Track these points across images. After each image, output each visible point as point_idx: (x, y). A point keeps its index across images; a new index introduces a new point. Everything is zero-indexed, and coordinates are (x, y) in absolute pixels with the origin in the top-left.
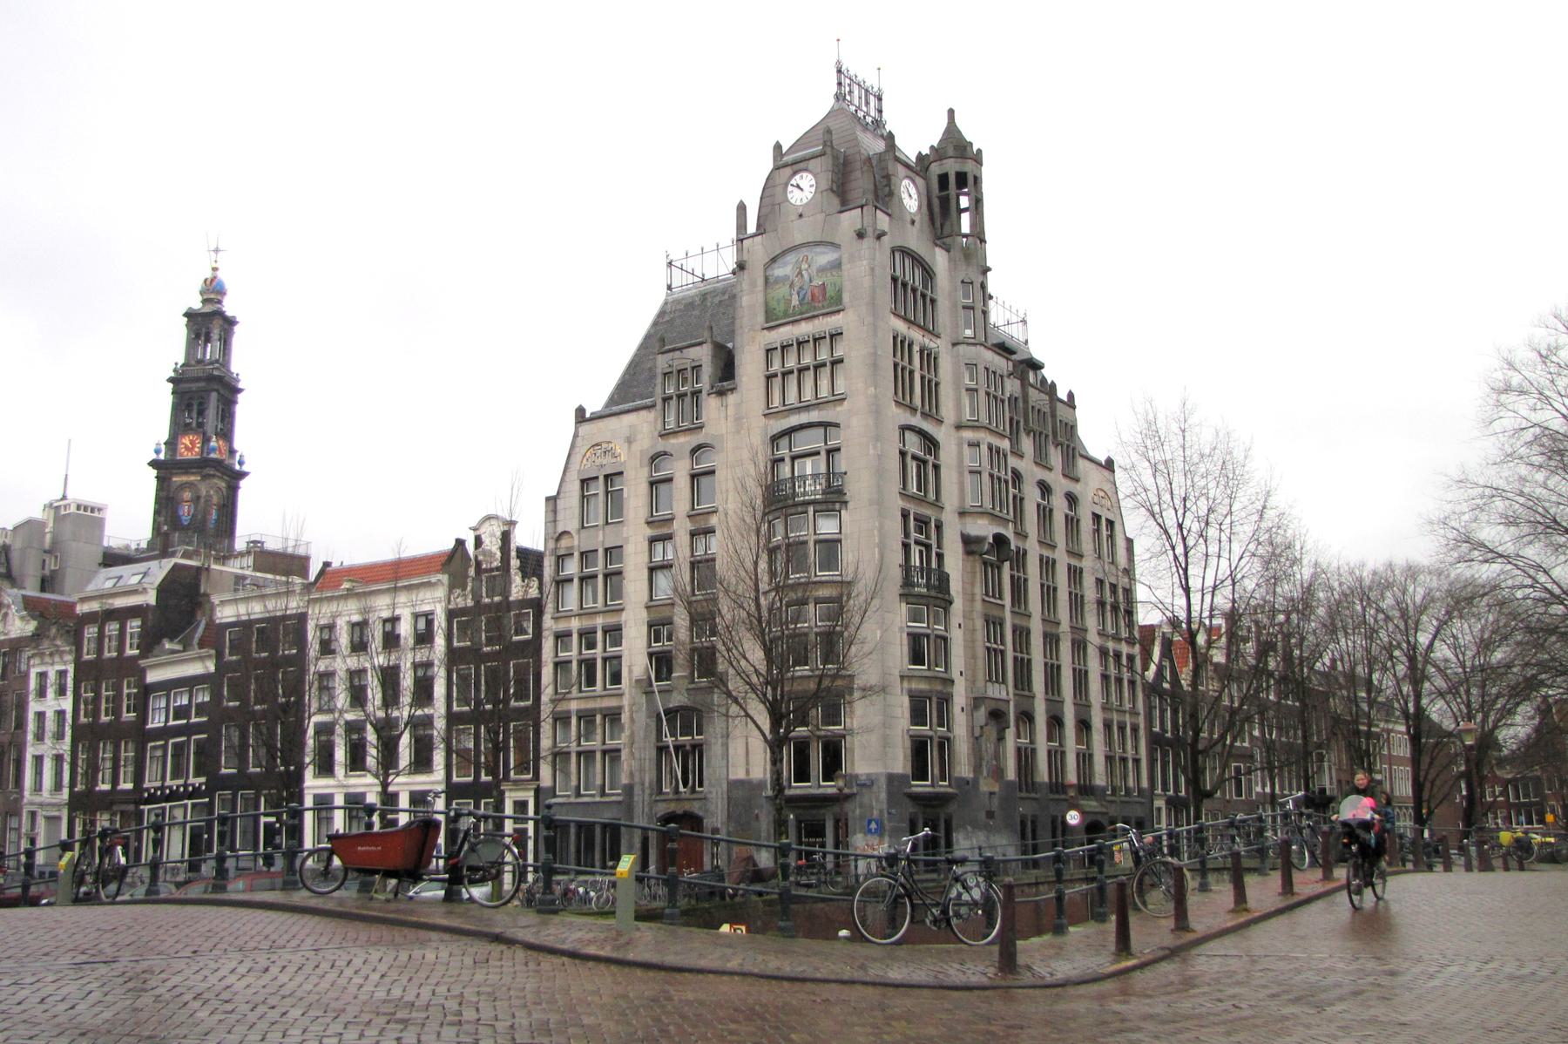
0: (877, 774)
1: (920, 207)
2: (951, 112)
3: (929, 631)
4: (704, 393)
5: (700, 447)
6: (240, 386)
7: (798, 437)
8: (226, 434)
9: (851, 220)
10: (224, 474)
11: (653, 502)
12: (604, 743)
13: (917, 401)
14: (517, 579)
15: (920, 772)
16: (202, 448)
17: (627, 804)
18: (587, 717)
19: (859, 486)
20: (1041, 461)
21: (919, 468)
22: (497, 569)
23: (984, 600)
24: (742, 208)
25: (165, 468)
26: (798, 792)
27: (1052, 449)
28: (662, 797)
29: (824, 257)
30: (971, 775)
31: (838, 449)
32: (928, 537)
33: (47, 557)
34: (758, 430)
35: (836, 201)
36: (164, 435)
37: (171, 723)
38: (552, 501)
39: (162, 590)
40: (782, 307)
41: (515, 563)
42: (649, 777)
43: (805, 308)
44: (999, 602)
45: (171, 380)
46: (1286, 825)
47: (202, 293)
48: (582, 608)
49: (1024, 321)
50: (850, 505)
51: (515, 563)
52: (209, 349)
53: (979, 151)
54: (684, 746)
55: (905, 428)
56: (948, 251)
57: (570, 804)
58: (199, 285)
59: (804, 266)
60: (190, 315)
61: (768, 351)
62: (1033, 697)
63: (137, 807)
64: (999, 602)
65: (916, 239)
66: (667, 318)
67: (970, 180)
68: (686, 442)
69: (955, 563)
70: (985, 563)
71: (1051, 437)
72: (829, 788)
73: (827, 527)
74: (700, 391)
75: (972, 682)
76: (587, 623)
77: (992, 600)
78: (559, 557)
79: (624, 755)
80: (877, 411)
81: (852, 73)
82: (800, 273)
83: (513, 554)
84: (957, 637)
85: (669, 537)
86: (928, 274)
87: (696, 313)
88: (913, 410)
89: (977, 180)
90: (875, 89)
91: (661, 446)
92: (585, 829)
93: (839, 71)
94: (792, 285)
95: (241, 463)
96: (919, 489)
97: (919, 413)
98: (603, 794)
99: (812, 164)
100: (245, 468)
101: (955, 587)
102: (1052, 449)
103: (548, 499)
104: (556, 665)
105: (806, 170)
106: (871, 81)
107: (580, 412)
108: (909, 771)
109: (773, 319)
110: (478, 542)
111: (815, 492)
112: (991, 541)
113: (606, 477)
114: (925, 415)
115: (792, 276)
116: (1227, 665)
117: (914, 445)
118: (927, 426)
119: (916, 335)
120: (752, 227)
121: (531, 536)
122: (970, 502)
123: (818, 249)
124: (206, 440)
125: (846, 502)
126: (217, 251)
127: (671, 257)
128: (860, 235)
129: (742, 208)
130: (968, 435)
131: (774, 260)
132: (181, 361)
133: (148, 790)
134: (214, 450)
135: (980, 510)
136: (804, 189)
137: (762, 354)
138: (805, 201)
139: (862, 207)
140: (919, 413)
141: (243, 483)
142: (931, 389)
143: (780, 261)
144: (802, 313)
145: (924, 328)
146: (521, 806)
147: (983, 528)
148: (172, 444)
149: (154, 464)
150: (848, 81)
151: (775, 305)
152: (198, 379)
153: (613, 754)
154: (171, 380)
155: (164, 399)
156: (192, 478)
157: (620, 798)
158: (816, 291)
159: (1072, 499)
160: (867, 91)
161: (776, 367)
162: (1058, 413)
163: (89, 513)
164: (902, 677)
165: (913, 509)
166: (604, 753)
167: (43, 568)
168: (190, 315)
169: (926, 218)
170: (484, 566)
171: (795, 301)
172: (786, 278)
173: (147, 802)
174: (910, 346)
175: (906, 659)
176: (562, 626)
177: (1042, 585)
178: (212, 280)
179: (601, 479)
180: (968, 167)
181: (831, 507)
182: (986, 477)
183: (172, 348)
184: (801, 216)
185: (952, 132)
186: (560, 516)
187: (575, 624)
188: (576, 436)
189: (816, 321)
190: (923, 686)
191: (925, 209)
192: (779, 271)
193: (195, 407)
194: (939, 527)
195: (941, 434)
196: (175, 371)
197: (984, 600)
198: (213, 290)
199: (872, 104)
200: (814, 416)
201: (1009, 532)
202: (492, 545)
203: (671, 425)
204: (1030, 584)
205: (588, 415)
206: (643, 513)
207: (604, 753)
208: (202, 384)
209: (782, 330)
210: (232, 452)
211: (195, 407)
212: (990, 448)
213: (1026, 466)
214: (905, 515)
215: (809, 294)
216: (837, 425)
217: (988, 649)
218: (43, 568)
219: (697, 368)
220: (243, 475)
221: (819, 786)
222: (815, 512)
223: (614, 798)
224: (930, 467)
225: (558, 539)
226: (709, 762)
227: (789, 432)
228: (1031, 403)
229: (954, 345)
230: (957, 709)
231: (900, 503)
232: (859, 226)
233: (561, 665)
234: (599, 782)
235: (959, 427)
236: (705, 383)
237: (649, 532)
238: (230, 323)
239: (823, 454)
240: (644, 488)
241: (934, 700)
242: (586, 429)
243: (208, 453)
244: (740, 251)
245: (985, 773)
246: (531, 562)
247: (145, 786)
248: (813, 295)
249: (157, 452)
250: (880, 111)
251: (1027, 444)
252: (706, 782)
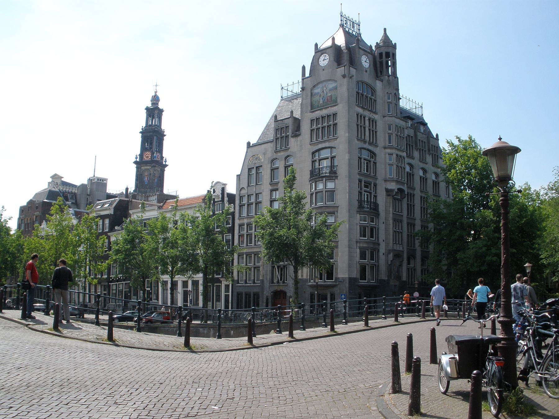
0: (346, 278)
1: (370, 66)
2: (385, 29)
3: (368, 225)
4: (290, 137)
5: (288, 156)
6: (165, 134)
7: (322, 152)
8: (160, 150)
9: (341, 71)
10: (159, 166)
11: (272, 177)
12: (255, 264)
13: (367, 138)
14: (227, 205)
15: (363, 277)
16: (151, 157)
17: (262, 286)
18: (248, 255)
19: (343, 170)
20: (422, 160)
21: (367, 163)
22: (220, 201)
23: (393, 213)
24: (304, 68)
25: (139, 164)
26: (328, 283)
27: (427, 156)
28: (274, 285)
29: (332, 85)
30: (387, 279)
31: (335, 157)
32: (370, 190)
33: (88, 197)
34: (308, 149)
35: (336, 64)
36: (138, 152)
38: (239, 176)
39: (116, 209)
40: (317, 104)
41: (226, 199)
42: (269, 277)
44: (400, 214)
45: (141, 132)
47: (151, 101)
48: (248, 215)
49: (421, 107)
50: (339, 178)
51: (226, 199)
52: (154, 121)
53: (395, 44)
54: (281, 266)
55: (361, 149)
56: (382, 81)
57: (243, 286)
58: (150, 98)
59: (325, 89)
60: (147, 109)
61: (312, 120)
62: (416, 250)
63: (108, 283)
64: (400, 214)
65: (367, 78)
67: (391, 55)
68: (283, 154)
69: (382, 200)
70: (395, 199)
71: (427, 151)
72: (329, 282)
73: (330, 185)
74: (288, 136)
75: (387, 244)
76: (249, 221)
77: (397, 213)
78: (241, 197)
79: (261, 269)
80: (350, 142)
81: (347, 16)
82: (323, 91)
83: (226, 196)
84: (382, 227)
85: (277, 190)
86: (373, 91)
88: (365, 142)
89: (394, 55)
90: (357, 22)
92: (248, 295)
93: (341, 16)
94: (320, 96)
95: (166, 161)
96: (367, 171)
97: (367, 143)
98: (246, 283)
100: (167, 163)
101: (382, 209)
102: (427, 156)
103: (237, 176)
104: (239, 236)
105: (325, 53)
106: (355, 18)
107: (249, 144)
108: (359, 276)
110: (214, 192)
111: (326, 173)
112: (396, 191)
113: (257, 167)
114: (370, 144)
117: (365, 155)
118: (370, 148)
119: (367, 113)
120: (307, 74)
121: (232, 189)
122: (388, 176)
123: (329, 82)
124: (153, 154)
125: (337, 177)
126: (156, 86)
127: (282, 86)
128: (344, 76)
129: (304, 68)
130: (389, 151)
131: (314, 87)
132: (144, 125)
133: (112, 278)
134: (155, 157)
135: (392, 179)
136: (324, 61)
137: (309, 121)
138: (325, 64)
139: (344, 66)
140: (367, 143)
141: (166, 169)
142: (373, 133)
143: (317, 87)
144: (323, 106)
145: (371, 111)
146: (227, 287)
147: (393, 186)
148: (141, 155)
149: (136, 163)
150: (345, 19)
152: (150, 132)
153: (257, 268)
154: (141, 132)
155: (138, 140)
156: (148, 167)
157: (259, 284)
158: (328, 98)
160: (353, 23)
161: (314, 127)
162: (431, 142)
163: (101, 182)
164: (357, 242)
165: (363, 179)
166: (255, 268)
167: (87, 201)
168: (147, 109)
169: (373, 70)
170: (216, 200)
171: (321, 102)
173: (111, 282)
174: (364, 117)
175: (359, 235)
176: (241, 222)
177: (421, 208)
178: (155, 96)
179: (255, 168)
180: (390, 50)
181: (331, 178)
182: (395, 166)
183: (141, 121)
184: (323, 70)
186: (241, 182)
187: (245, 221)
188: (247, 152)
189: (328, 109)
190: (365, 245)
191: (372, 66)
192: (316, 91)
193: (149, 142)
194: (375, 185)
195: (377, 151)
196: (142, 129)
197: (393, 213)
198: (155, 99)
199: (356, 28)
200: (327, 144)
201: (405, 188)
202: (218, 192)
204: (416, 207)
205: (251, 145)
206: (269, 181)
207: (255, 268)
208: (151, 134)
209: (316, 112)
210: (162, 158)
211: (149, 142)
212: (397, 155)
213: (415, 162)
214: (360, 181)
216: (335, 148)
217: (395, 231)
218: (87, 201)
219: (287, 127)
220: (166, 166)
221: (325, 282)
222: (326, 180)
223: (257, 284)
224: (372, 163)
225: (241, 190)
226: (289, 272)
227: (319, 150)
228: (419, 138)
229: (384, 117)
230: (381, 254)
231: (358, 177)
232: (344, 74)
233: (241, 236)
234: (252, 278)
235: (385, 148)
236: (290, 133)
237: (270, 188)
238: (162, 111)
239: (330, 158)
240: (269, 171)
241: (369, 250)
242: (250, 149)
243: (153, 159)
244: (303, 83)
245: (393, 278)
246: (231, 198)
247: (110, 277)
248: (327, 99)
249: (136, 158)
250: (359, 30)
251: (416, 154)
252: (287, 280)
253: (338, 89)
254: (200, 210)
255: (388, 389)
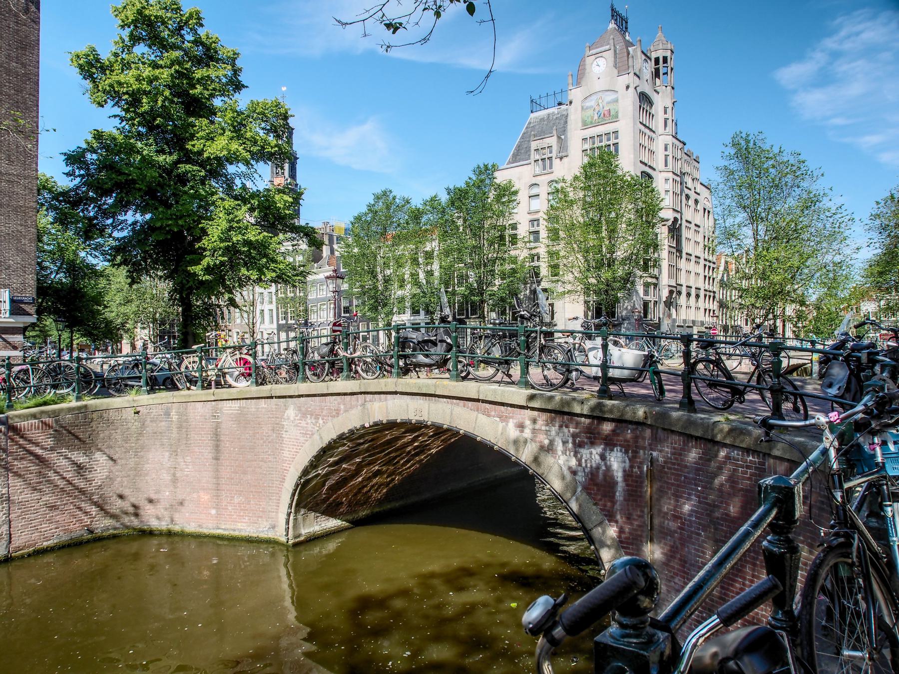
4: (554, 158)
29: (610, 97)
35: (616, 71)
40: (590, 120)
59: (600, 101)
87: (545, 123)
91: (534, 181)
93: (612, 10)
99: (604, 54)
107: (394, 33)
109: (586, 125)
115: (595, 106)
116: (73, 285)
143: (589, 99)
158: (606, 113)
171: (596, 117)
172: (591, 107)
185: (244, 86)
215: (602, 114)
253: (619, 101)
254: (447, 232)
255: (412, 381)
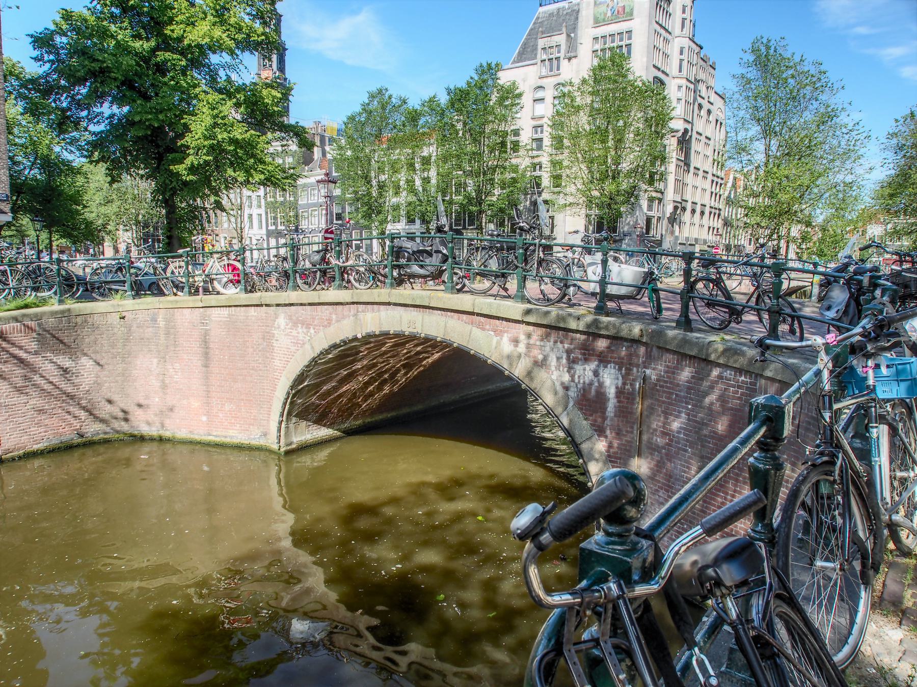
37: (310, 202)
40: (602, 17)
43: (613, 18)
46: (704, 512)
66: (540, 21)
87: (555, 18)
109: (598, 23)
151: (599, 16)
158: (620, 9)
159: (709, 112)
171: (609, 14)
203: (544, 74)
209: (602, 28)
